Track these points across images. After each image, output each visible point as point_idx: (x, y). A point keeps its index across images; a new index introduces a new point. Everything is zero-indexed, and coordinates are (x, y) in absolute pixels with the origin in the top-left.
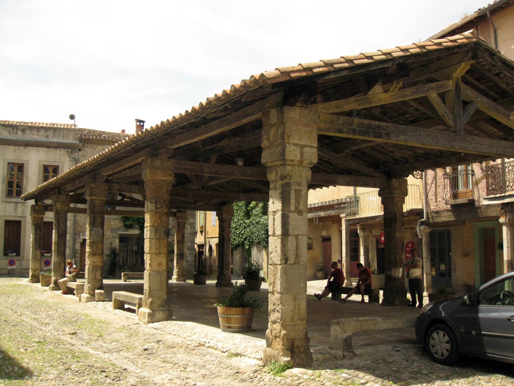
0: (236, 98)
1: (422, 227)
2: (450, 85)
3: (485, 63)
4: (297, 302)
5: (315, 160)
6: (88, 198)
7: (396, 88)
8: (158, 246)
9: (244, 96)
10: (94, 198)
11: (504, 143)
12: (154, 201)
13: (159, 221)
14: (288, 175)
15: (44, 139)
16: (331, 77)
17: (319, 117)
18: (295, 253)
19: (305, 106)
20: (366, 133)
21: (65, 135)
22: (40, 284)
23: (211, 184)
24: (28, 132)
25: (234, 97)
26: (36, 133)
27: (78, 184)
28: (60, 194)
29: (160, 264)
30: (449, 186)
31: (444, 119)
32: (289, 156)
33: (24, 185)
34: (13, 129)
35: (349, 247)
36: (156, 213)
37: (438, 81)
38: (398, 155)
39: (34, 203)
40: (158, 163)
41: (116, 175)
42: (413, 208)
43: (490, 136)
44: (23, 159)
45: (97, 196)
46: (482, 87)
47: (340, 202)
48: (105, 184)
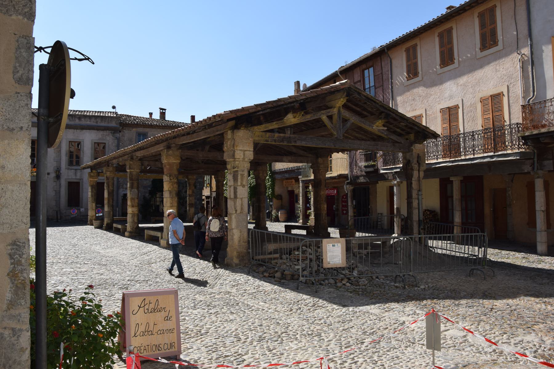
1: (348, 186)
2: (335, 110)
6: (128, 171)
10: (132, 170)
12: (168, 175)
13: (172, 187)
15: (95, 124)
20: (282, 141)
21: (109, 121)
22: (93, 227)
24: (83, 119)
28: (108, 166)
36: (170, 182)
39: (90, 171)
40: (170, 152)
42: (342, 173)
44: (80, 138)
45: (134, 169)
47: (298, 168)
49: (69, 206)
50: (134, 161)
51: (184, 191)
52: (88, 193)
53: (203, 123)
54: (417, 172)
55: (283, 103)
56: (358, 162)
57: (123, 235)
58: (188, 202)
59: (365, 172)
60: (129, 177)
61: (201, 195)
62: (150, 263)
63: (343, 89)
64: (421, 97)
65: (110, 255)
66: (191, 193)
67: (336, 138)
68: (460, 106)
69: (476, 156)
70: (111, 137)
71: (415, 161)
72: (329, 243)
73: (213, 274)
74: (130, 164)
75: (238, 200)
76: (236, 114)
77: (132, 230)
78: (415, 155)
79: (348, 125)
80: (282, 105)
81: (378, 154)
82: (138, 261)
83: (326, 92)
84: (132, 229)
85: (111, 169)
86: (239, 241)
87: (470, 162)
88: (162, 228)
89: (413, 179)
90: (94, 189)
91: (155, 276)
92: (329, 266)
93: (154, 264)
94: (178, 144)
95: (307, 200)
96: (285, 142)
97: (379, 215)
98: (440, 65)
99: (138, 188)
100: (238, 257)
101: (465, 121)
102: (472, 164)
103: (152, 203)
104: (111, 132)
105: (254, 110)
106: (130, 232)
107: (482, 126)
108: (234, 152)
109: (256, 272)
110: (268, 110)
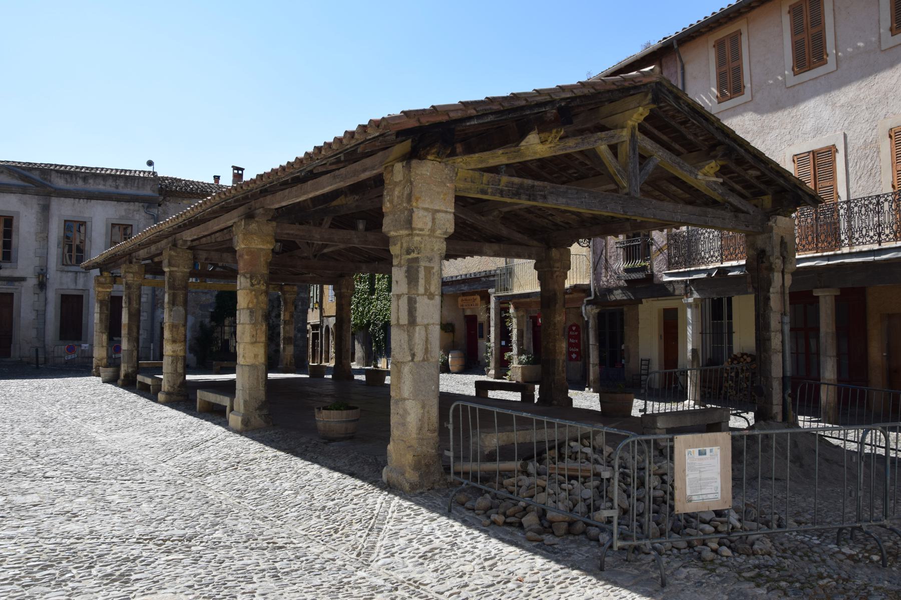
0: (351, 147)
1: (589, 308)
2: (625, 134)
3: (668, 108)
4: (426, 410)
5: (451, 229)
6: (166, 269)
7: (555, 138)
8: (255, 333)
9: (362, 146)
11: (689, 208)
12: (248, 276)
13: (255, 301)
14: (416, 248)
15: (113, 190)
16: (472, 123)
17: (457, 174)
18: (424, 347)
19: (439, 160)
20: (517, 194)
21: (140, 185)
22: (100, 379)
23: (325, 251)
24: (91, 181)
25: (348, 146)
26: (102, 182)
27: (153, 248)
28: (131, 262)
29: (256, 356)
30: (622, 257)
31: (615, 177)
32: (417, 223)
33: (86, 249)
34: (71, 177)
35: (499, 330)
36: (251, 291)
37: (609, 129)
38: (558, 219)
39: (99, 274)
40: (253, 226)
41: (204, 239)
42: (578, 283)
43: (675, 199)
44: (85, 215)
45: (178, 267)
46: (665, 138)
48: (188, 251)
49: (61, 339)
50: (179, 250)
51: (273, 314)
52: (95, 316)
53: (334, 147)
54: (781, 274)
55: (523, 103)
56: (611, 261)
57: (155, 400)
58: (282, 335)
59: (626, 281)
60: (169, 282)
61: (305, 322)
62: (202, 474)
63: (645, 85)
64: (748, 132)
65: (117, 447)
66: (287, 318)
67: (627, 194)
68: (841, 148)
69: (885, 245)
70: (143, 214)
71: (777, 251)
72: (690, 447)
73: (359, 514)
74: (170, 257)
75: (417, 328)
76: (419, 120)
77: (171, 390)
78: (776, 240)
79: (650, 167)
80: (522, 108)
81: (654, 247)
82: (175, 466)
83: (615, 87)
84: (172, 387)
85: (135, 268)
86: (420, 429)
87: (871, 258)
88: (232, 383)
89: (771, 290)
90: (104, 308)
91: (211, 518)
92: (690, 509)
93: (213, 476)
94: (272, 209)
95: (504, 334)
96: (523, 196)
97: (643, 362)
98: (793, 70)
99: (185, 303)
100: (417, 467)
101: (852, 177)
102: (875, 261)
103: (215, 335)
104: (143, 206)
105: (459, 115)
106: (168, 394)
107: (893, 186)
108: (411, 212)
109: (468, 509)
110: (491, 118)
